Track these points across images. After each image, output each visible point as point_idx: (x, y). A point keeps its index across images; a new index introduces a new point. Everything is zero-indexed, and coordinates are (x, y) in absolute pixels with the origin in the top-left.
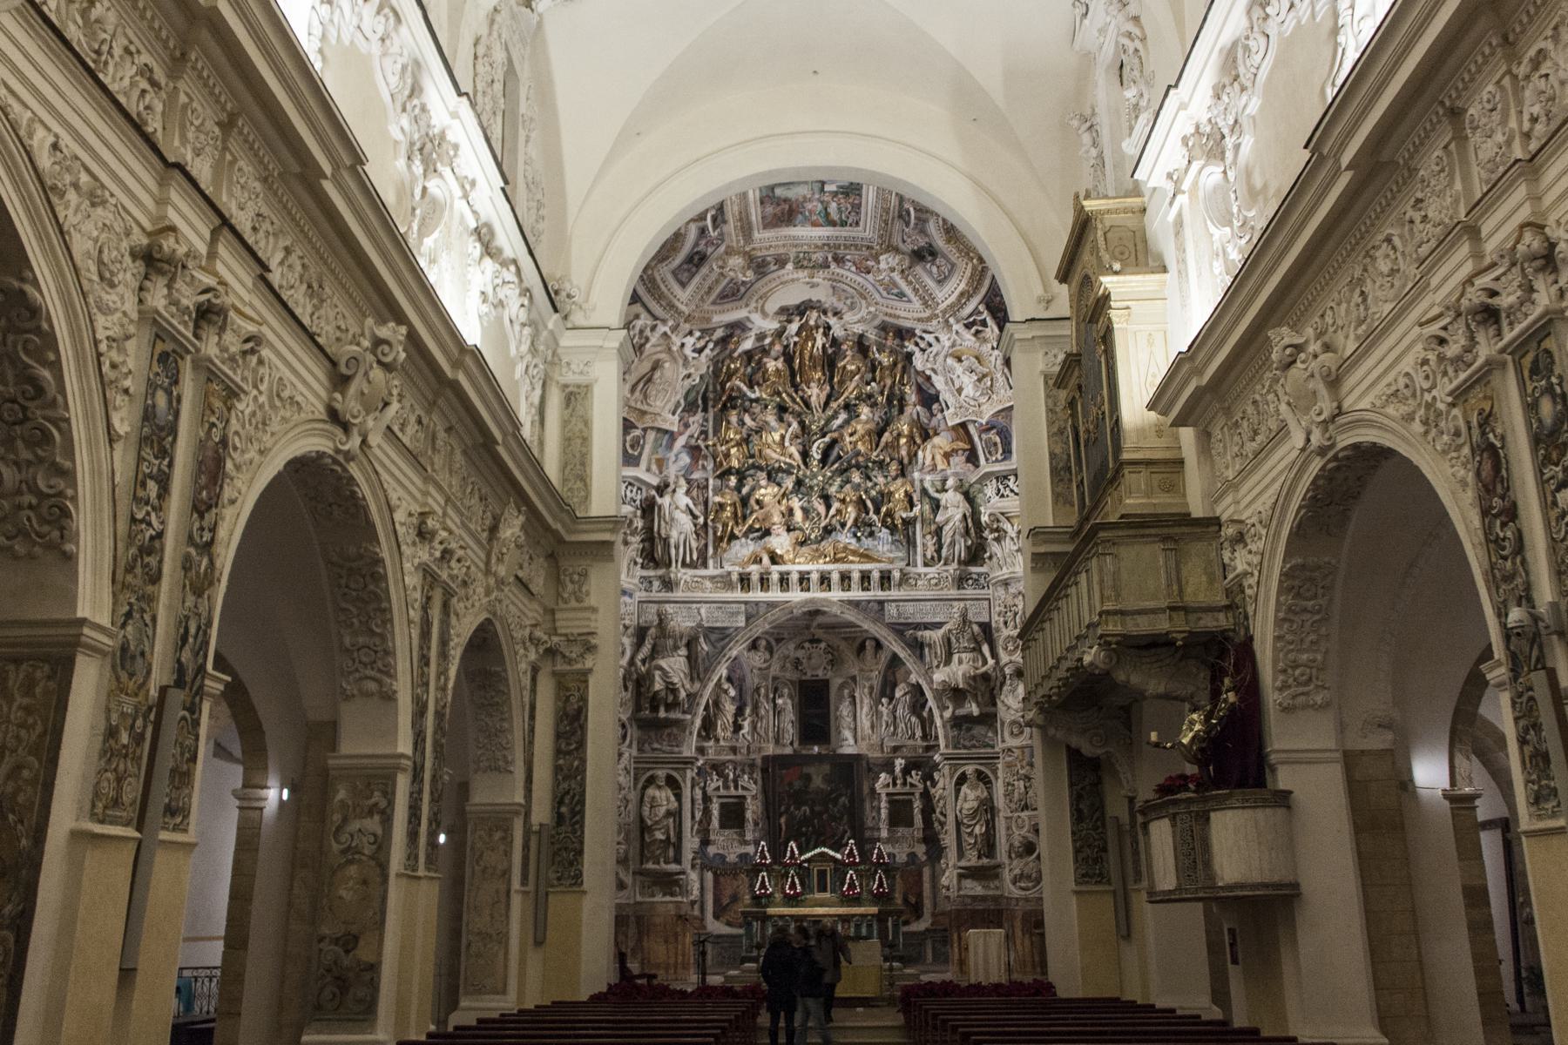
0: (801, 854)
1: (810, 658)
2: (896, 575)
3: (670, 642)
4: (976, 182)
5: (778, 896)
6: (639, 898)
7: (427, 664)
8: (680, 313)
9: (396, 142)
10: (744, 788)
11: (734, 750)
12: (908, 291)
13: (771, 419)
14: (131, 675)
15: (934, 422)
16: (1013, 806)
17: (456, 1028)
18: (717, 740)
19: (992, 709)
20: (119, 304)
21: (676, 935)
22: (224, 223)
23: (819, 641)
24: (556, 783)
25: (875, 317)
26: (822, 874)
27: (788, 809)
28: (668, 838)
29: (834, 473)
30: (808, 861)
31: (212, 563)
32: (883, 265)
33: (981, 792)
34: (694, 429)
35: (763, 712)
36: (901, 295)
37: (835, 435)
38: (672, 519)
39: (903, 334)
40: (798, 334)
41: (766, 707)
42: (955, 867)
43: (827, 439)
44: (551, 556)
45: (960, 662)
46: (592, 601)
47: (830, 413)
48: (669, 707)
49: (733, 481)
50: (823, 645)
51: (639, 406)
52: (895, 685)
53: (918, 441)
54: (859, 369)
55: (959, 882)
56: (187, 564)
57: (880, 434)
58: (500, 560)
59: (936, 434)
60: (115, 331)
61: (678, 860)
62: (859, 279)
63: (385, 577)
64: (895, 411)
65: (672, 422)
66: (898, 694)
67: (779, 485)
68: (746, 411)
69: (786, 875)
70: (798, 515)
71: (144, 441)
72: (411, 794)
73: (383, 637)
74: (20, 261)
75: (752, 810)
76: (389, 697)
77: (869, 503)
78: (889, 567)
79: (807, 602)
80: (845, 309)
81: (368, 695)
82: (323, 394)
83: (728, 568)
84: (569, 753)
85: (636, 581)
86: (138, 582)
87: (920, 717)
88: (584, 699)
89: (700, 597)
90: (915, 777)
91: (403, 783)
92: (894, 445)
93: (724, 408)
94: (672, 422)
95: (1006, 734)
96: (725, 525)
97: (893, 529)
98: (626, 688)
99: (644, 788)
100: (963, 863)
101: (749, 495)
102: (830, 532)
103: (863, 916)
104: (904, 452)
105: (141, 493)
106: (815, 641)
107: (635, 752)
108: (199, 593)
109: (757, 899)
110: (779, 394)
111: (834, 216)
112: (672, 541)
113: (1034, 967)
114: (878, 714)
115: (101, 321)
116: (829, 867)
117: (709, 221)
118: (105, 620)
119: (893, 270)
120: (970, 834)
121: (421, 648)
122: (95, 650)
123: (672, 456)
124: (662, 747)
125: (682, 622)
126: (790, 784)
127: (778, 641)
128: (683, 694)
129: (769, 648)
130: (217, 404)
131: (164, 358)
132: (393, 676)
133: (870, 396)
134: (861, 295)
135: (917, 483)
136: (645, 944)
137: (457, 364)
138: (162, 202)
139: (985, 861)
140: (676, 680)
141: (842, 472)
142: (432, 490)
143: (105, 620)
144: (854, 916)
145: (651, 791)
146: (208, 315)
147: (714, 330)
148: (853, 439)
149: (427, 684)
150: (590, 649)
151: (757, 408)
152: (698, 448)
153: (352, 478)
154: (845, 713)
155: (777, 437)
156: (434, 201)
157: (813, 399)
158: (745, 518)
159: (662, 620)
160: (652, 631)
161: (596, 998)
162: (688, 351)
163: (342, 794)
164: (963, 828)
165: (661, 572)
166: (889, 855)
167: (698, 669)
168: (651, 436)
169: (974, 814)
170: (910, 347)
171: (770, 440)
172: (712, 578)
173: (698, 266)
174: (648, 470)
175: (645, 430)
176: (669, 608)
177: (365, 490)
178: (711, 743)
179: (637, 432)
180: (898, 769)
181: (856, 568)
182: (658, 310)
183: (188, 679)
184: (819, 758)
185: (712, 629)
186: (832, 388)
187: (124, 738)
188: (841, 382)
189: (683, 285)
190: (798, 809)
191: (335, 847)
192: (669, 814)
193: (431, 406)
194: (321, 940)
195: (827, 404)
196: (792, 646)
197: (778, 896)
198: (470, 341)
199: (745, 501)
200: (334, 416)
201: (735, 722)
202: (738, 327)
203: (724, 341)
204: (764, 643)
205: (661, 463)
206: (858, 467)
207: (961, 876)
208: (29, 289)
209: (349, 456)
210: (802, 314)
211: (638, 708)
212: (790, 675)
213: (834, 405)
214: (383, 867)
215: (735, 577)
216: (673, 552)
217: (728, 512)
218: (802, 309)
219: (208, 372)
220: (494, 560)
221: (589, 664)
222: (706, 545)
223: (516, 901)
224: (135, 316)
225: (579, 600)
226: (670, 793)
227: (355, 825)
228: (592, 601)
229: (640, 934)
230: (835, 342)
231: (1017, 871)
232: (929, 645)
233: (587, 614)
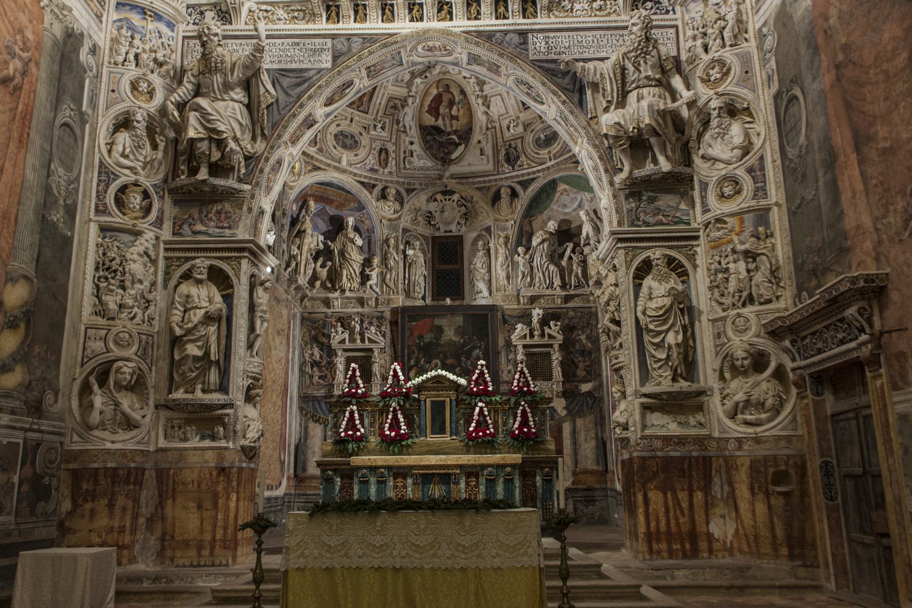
0: (408, 379)
3: (218, 79)
6: (162, 443)
10: (370, 340)
11: (361, 302)
16: (727, 301)
17: (598, 464)
19: (688, 170)
23: (452, 193)
26: (438, 408)
27: (418, 361)
28: (207, 354)
30: (419, 388)
33: (674, 282)
35: (392, 263)
41: (395, 258)
42: (637, 394)
45: (640, 98)
50: (456, 197)
52: (530, 235)
55: (643, 417)
61: (223, 388)
66: (535, 242)
87: (558, 265)
90: (554, 328)
95: (712, 199)
98: (155, 147)
100: (649, 388)
103: (500, 467)
106: (447, 193)
107: (166, 233)
113: (775, 546)
114: (515, 265)
116: (448, 397)
120: (658, 346)
124: (208, 230)
125: (233, 53)
126: (421, 337)
127: (409, 191)
129: (400, 199)
136: (168, 510)
139: (683, 385)
144: (484, 467)
154: (479, 265)
164: (646, 338)
167: (264, 121)
169: (664, 316)
178: (337, 294)
180: (535, 320)
184: (452, 310)
185: (284, 72)
192: (209, 319)
196: (423, 197)
197: (374, 440)
201: (362, 273)
204: (393, 191)
207: (645, 408)
229: (162, 497)
231: (740, 397)
232: (595, 86)
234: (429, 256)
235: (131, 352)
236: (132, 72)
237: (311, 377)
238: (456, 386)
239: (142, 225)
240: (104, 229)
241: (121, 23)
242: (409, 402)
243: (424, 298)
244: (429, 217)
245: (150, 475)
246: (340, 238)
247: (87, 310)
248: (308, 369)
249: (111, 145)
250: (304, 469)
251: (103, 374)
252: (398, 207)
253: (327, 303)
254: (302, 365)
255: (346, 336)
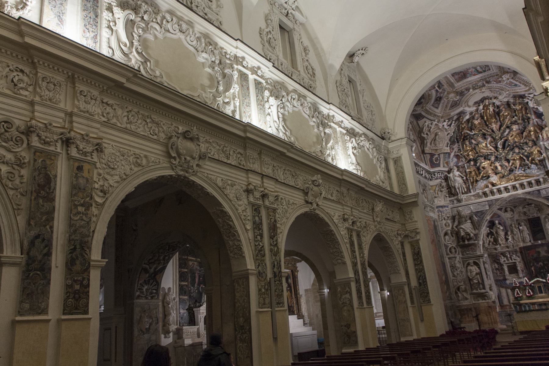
0: (530, 281)
1: (529, 211)
2: (541, 180)
3: (464, 219)
4: (512, 53)
5: (524, 296)
6: (474, 302)
7: (355, 252)
8: (439, 116)
9: (313, 126)
10: (514, 259)
11: (508, 247)
12: (518, 83)
13: (480, 140)
14: (262, 277)
15: (544, 123)
18: (500, 245)
20: (243, 205)
21: (490, 313)
22: (263, 176)
23: (531, 204)
24: (417, 274)
25: (510, 95)
26: (539, 288)
27: (533, 264)
28: (479, 282)
29: (508, 151)
30: (533, 283)
31: (278, 248)
32: (504, 79)
34: (456, 149)
35: (515, 232)
36: (516, 85)
37: (505, 138)
38: (455, 180)
39: (522, 97)
40: (483, 109)
41: (516, 231)
43: (502, 140)
44: (400, 209)
46: (415, 219)
47: (501, 131)
48: (468, 240)
49: (472, 163)
50: (533, 205)
51: (434, 148)
53: (538, 131)
54: (509, 113)
56: (271, 250)
57: (522, 133)
58: (377, 217)
59: (546, 126)
60: (244, 209)
61: (484, 288)
62: (498, 85)
63: (335, 234)
64: (527, 123)
65: (448, 150)
67: (489, 160)
68: (472, 139)
69: (525, 289)
70: (499, 168)
71: (254, 229)
72: (356, 287)
73: (339, 248)
74: (220, 205)
75: (520, 266)
76: (344, 263)
77: (524, 158)
78: (538, 178)
79: (510, 196)
80: (498, 95)
81: (340, 263)
82: (303, 198)
83: (477, 191)
84: (418, 264)
85: (448, 202)
86: (260, 258)
88: (419, 248)
89: (471, 202)
91: (353, 285)
92: (529, 135)
93: (464, 140)
94: (448, 150)
96: (473, 178)
97: (536, 164)
98: (453, 236)
99: (467, 267)
101: (479, 166)
102: (513, 171)
104: (533, 137)
105: (256, 239)
107: (461, 256)
108: (275, 255)
109: (516, 298)
110: (481, 130)
111: (480, 70)
112: (456, 187)
115: (240, 208)
116: (542, 285)
117: (437, 88)
118: (254, 268)
119: (508, 79)
121: (351, 249)
122: (252, 274)
123: (450, 160)
126: (532, 256)
127: (515, 207)
128: (472, 235)
129: (512, 210)
130: (271, 214)
131: (255, 210)
132: (344, 258)
133: (516, 121)
134: (501, 90)
135: (543, 146)
137: (342, 175)
138: (248, 178)
140: (468, 231)
141: (512, 149)
142: (345, 207)
143: (254, 268)
145: (469, 268)
146: (264, 196)
147: (453, 117)
148: (512, 138)
149: (356, 257)
150: (418, 233)
151: (475, 137)
152: (458, 155)
153: (317, 214)
155: (484, 145)
156: (328, 134)
157: (494, 129)
158: (480, 173)
159: (459, 213)
160: (457, 217)
161: (442, 336)
162: (446, 127)
163: (339, 289)
165: (456, 197)
166: (519, 283)
167: (476, 226)
168: (442, 156)
170: (526, 100)
171: (482, 146)
172: (473, 195)
173: (440, 101)
174: (444, 167)
175: (439, 155)
176: (460, 209)
177: (322, 215)
178: (498, 246)
179: (436, 156)
181: (525, 181)
182: (432, 118)
183: (277, 274)
184: (542, 245)
186: (501, 122)
187: (263, 290)
188: (503, 120)
189: (437, 108)
190: (538, 264)
191: (341, 303)
192: (477, 274)
193: (340, 186)
194: (342, 326)
195: (500, 129)
196: (521, 208)
197: (524, 296)
198: (343, 168)
199: (478, 169)
200: (307, 202)
201: (505, 238)
202: (462, 113)
203: (458, 119)
204: (509, 209)
205: (447, 163)
206: (517, 146)
208: (223, 209)
209: (314, 209)
210: (483, 102)
211: (458, 242)
212: (523, 218)
213: (502, 128)
214: (352, 306)
215: (481, 194)
216: (458, 190)
217: (473, 173)
218: (482, 100)
219: (267, 208)
220: (375, 217)
221: (418, 238)
222: (469, 185)
223: (410, 310)
224: (247, 204)
225: (411, 219)
226: (476, 267)
227: (344, 297)
228: (415, 219)
230: (498, 107)
233: (415, 223)
234: (528, 226)
235: (462, 284)
236: (444, 222)
237: (497, 274)
238: (543, 282)
239: (456, 255)
240: (449, 258)
241: (439, 211)
242: (532, 287)
243: (530, 241)
244: (525, 213)
245: (473, 309)
246: (495, 228)
247: (451, 276)
248: (495, 271)
249: (445, 239)
250: (503, 303)
251: (458, 289)
252: (512, 213)
253: (496, 249)
254: (493, 270)
255: (505, 259)
